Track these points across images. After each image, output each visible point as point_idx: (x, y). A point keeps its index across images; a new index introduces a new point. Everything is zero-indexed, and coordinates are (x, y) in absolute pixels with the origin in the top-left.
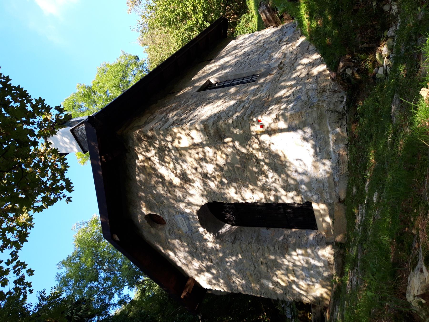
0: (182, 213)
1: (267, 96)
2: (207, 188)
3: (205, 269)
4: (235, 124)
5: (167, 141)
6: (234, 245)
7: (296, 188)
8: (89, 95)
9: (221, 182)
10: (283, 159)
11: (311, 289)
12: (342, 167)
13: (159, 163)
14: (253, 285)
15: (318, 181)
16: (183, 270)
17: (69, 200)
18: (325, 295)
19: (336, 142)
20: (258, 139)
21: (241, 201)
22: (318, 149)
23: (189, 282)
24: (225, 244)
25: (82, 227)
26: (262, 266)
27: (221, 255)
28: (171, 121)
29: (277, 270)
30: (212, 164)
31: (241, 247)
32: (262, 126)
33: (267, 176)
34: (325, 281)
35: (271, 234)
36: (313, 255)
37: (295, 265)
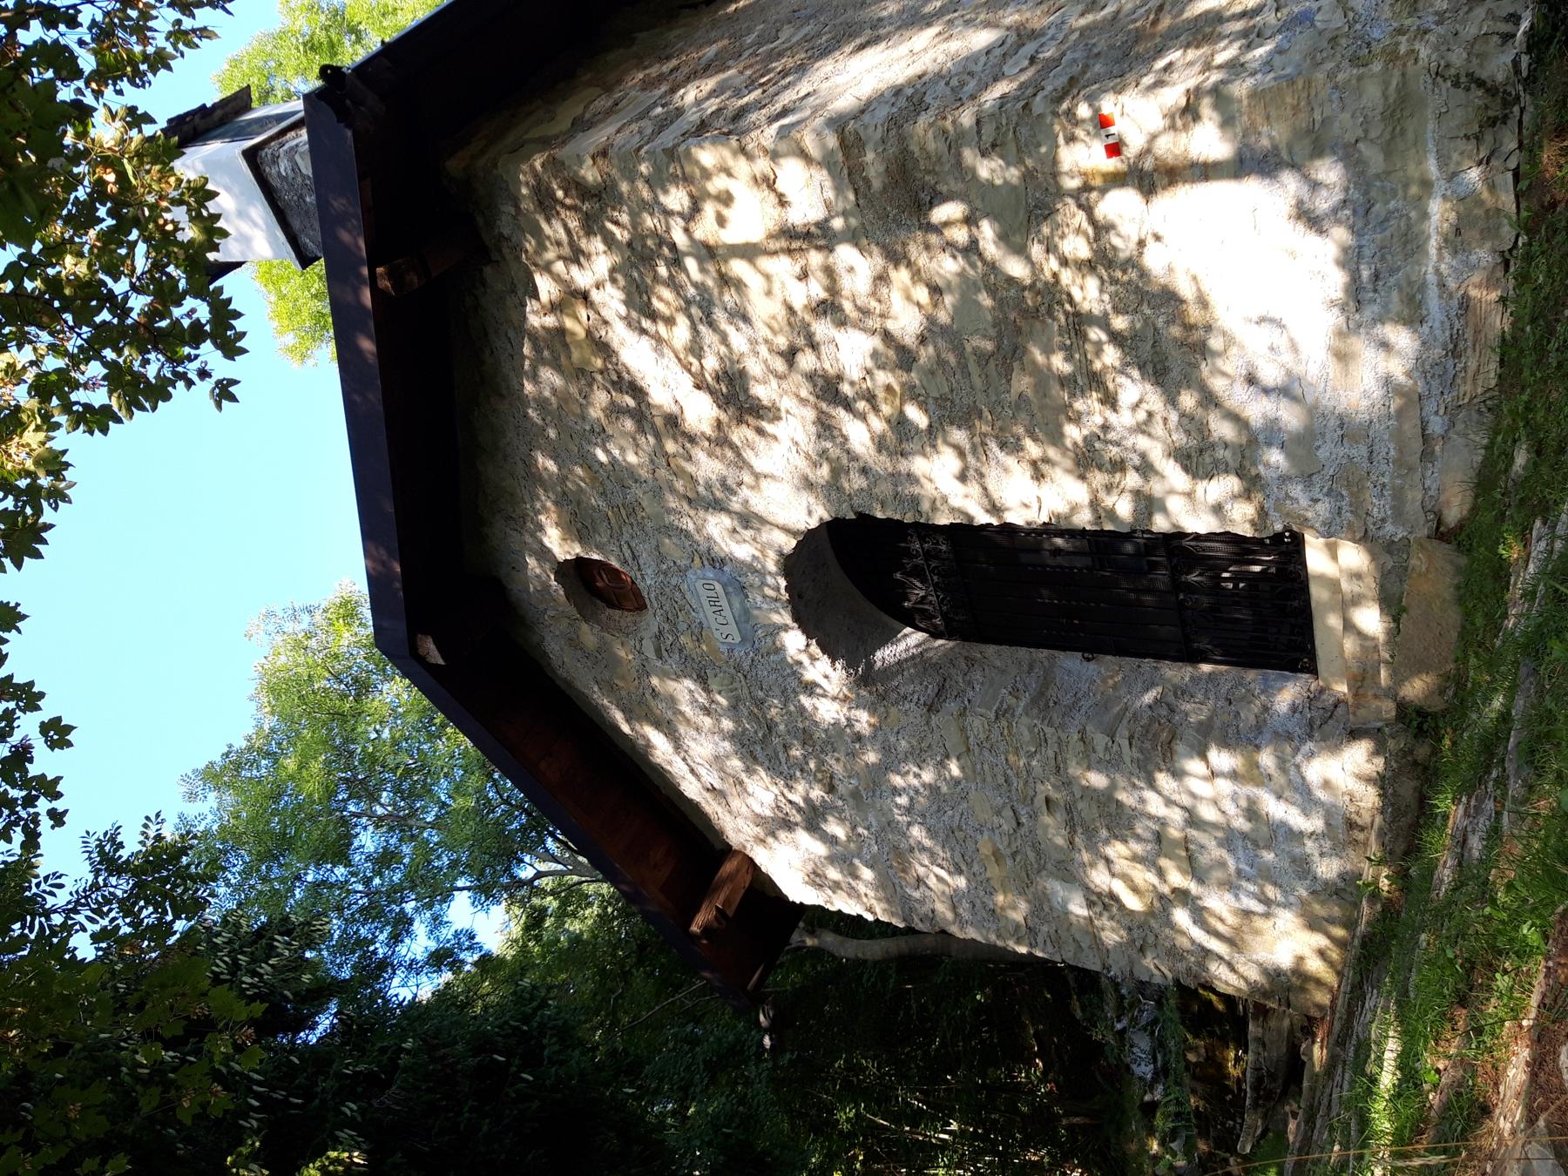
0: (718, 562)
1: (1148, 12)
2: (834, 452)
3: (798, 818)
4: (988, 132)
5: (668, 213)
6: (934, 720)
7: (1242, 461)
8: (332, 45)
9: (900, 423)
10: (1194, 314)
11: (1257, 932)
12: (1472, 364)
13: (627, 320)
14: (1000, 898)
15: (1347, 429)
16: (704, 817)
17: (224, 392)
18: (1315, 965)
19: (1456, 240)
20: (1089, 210)
21: (982, 518)
22: (1365, 274)
23: (729, 867)
24: (893, 710)
25: (289, 627)
26: (1047, 819)
27: (872, 757)
28: (693, 117)
29: (1116, 838)
30: (864, 330)
31: (963, 729)
32: (1114, 150)
33: (1110, 401)
34: (1323, 903)
35: (1104, 681)
36: (1279, 779)
37: (1193, 820)
